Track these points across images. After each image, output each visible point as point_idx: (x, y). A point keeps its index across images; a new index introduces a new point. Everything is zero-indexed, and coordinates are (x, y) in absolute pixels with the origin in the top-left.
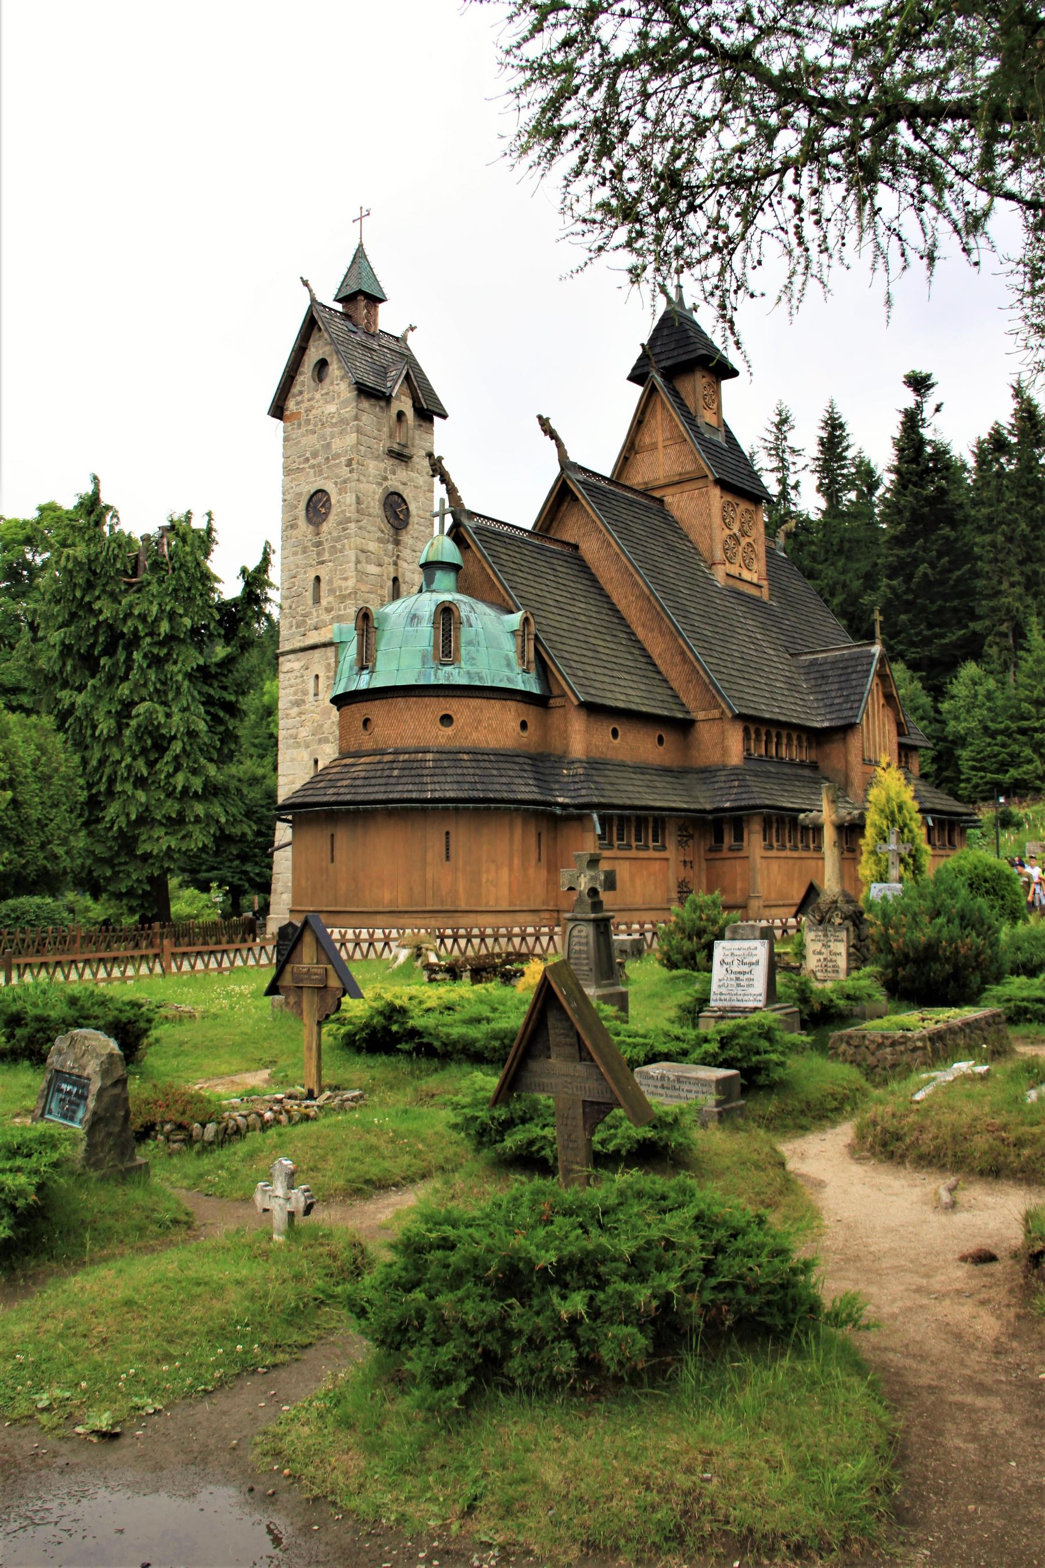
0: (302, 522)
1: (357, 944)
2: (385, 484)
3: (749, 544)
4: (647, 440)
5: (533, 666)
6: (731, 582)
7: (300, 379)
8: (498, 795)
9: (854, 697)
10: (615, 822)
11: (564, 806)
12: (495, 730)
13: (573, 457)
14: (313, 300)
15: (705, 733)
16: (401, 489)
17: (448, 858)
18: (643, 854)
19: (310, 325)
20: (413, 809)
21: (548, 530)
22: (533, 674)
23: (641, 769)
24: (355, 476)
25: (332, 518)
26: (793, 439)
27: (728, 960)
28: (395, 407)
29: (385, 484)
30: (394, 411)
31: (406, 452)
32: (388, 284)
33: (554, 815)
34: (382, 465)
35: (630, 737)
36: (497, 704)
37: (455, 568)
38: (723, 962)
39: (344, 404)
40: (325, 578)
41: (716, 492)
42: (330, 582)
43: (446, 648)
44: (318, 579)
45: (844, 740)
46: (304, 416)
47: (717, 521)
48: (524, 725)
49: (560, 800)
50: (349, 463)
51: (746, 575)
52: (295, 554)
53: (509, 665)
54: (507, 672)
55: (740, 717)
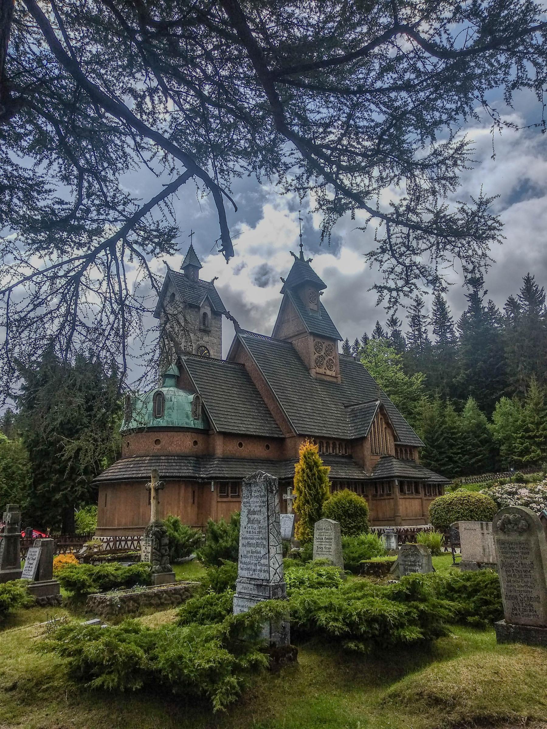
6: (319, 376)
8: (171, 474)
10: (230, 485)
11: (203, 478)
15: (289, 443)
16: (205, 345)
22: (200, 421)
28: (202, 311)
29: (198, 343)
36: (182, 434)
37: (178, 377)
43: (158, 412)
45: (362, 445)
47: (312, 350)
48: (195, 443)
51: (328, 372)
53: (188, 417)
54: (187, 421)
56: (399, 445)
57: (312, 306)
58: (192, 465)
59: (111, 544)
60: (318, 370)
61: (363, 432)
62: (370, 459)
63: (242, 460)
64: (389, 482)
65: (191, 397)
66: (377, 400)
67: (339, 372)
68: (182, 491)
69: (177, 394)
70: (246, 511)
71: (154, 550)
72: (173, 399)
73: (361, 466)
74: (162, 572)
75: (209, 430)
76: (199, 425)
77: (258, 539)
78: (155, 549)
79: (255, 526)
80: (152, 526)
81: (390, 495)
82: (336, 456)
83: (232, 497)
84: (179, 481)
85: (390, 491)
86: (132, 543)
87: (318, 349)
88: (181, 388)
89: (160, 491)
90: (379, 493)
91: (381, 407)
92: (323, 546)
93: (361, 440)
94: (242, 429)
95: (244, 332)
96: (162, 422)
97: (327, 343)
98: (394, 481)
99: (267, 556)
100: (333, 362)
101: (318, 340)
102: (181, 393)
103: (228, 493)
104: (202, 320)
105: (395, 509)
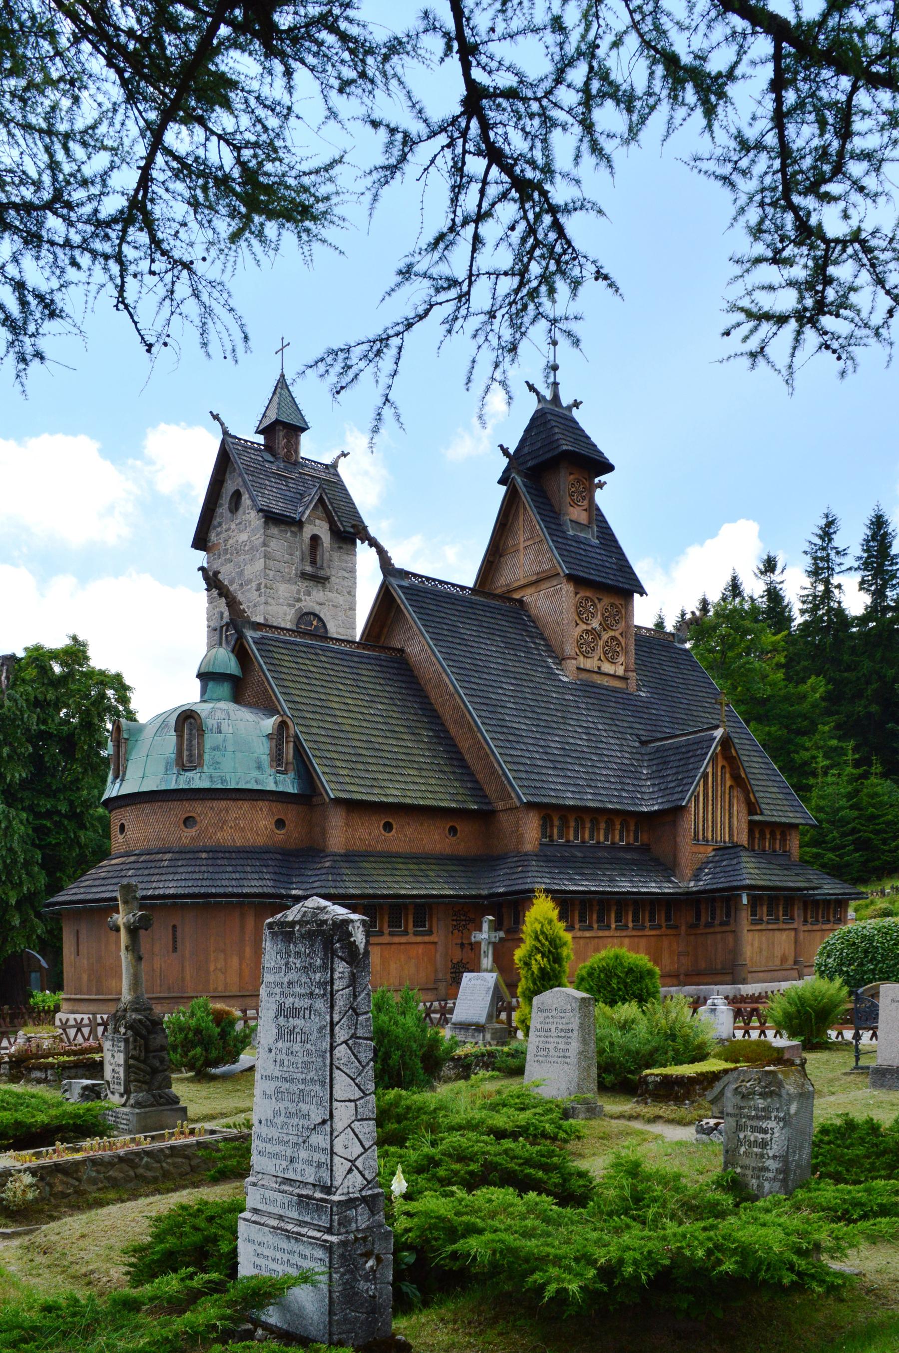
1: (79, 1030)
2: (298, 605)
3: (613, 638)
4: (510, 542)
5: (291, 767)
6: (584, 676)
8: (221, 890)
13: (398, 562)
14: (225, 433)
15: (506, 821)
16: (317, 609)
17: (175, 949)
18: (396, 939)
21: (378, 637)
22: (291, 774)
23: (420, 859)
24: (263, 599)
26: (838, 541)
28: (308, 531)
29: (298, 605)
31: (321, 573)
34: (294, 588)
35: (409, 831)
36: (246, 805)
41: (567, 588)
46: (222, 547)
48: (280, 824)
49: (294, 892)
50: (258, 589)
51: (607, 668)
53: (259, 767)
54: (257, 774)
55: (531, 805)
56: (760, 822)
57: (578, 514)
58: (271, 869)
59: (86, 1031)
60: (583, 662)
61: (676, 797)
62: (689, 853)
63: (389, 859)
64: (728, 899)
65: (269, 724)
66: (717, 727)
67: (632, 667)
69: (232, 716)
70: (275, 1007)
71: (131, 1062)
72: (224, 728)
73: (667, 867)
74: (152, 1105)
75: (311, 797)
76: (288, 784)
77: (304, 1081)
78: (133, 1057)
79: (297, 1047)
80: (125, 1010)
81: (726, 923)
82: (614, 847)
83: (416, 934)
84: (241, 904)
85: (728, 915)
87: (581, 613)
88: (248, 705)
89: (142, 932)
90: (703, 919)
91: (726, 742)
92: (551, 1046)
93: (675, 812)
96: (197, 780)
98: (740, 896)
99: (327, 1127)
100: (619, 644)
104: (307, 552)
105: (735, 952)
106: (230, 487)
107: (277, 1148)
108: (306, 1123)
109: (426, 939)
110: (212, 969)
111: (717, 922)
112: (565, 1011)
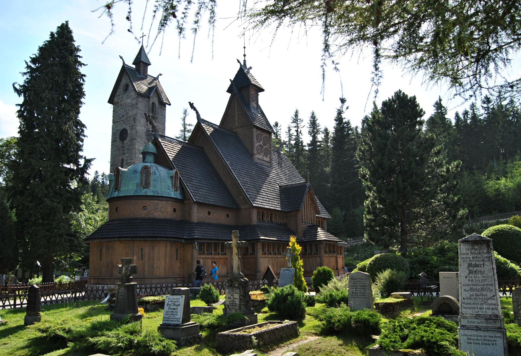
0: (118, 140)
2: (147, 127)
3: (266, 148)
5: (178, 189)
6: (259, 161)
7: (119, 90)
9: (300, 201)
10: (206, 245)
11: (185, 239)
12: (163, 212)
13: (202, 117)
17: (101, 260)
19: (125, 69)
20: (129, 240)
22: (179, 192)
25: (128, 138)
27: (170, 303)
29: (147, 127)
30: (151, 102)
31: (155, 116)
32: (151, 57)
33: (181, 242)
36: (164, 202)
38: (168, 304)
39: (133, 99)
40: (125, 159)
41: (255, 130)
42: (127, 160)
44: (123, 160)
48: (175, 210)
49: (185, 237)
51: (265, 159)
52: (115, 151)
53: (169, 189)
54: (168, 191)
68: (169, 248)
71: (241, 297)
76: (177, 195)
77: (483, 285)
79: (479, 275)
81: (317, 254)
83: (222, 254)
86: (151, 290)
92: (358, 292)
94: (211, 201)
95: (204, 121)
97: (265, 135)
101: (259, 132)
102: (161, 168)
103: (204, 252)
106: (124, 82)
107: (473, 306)
108: (486, 297)
109: (225, 257)
110: (155, 266)
111: (313, 253)
112: (362, 279)
